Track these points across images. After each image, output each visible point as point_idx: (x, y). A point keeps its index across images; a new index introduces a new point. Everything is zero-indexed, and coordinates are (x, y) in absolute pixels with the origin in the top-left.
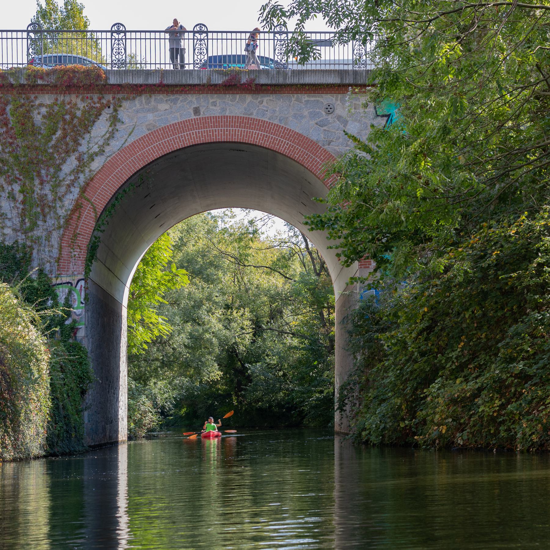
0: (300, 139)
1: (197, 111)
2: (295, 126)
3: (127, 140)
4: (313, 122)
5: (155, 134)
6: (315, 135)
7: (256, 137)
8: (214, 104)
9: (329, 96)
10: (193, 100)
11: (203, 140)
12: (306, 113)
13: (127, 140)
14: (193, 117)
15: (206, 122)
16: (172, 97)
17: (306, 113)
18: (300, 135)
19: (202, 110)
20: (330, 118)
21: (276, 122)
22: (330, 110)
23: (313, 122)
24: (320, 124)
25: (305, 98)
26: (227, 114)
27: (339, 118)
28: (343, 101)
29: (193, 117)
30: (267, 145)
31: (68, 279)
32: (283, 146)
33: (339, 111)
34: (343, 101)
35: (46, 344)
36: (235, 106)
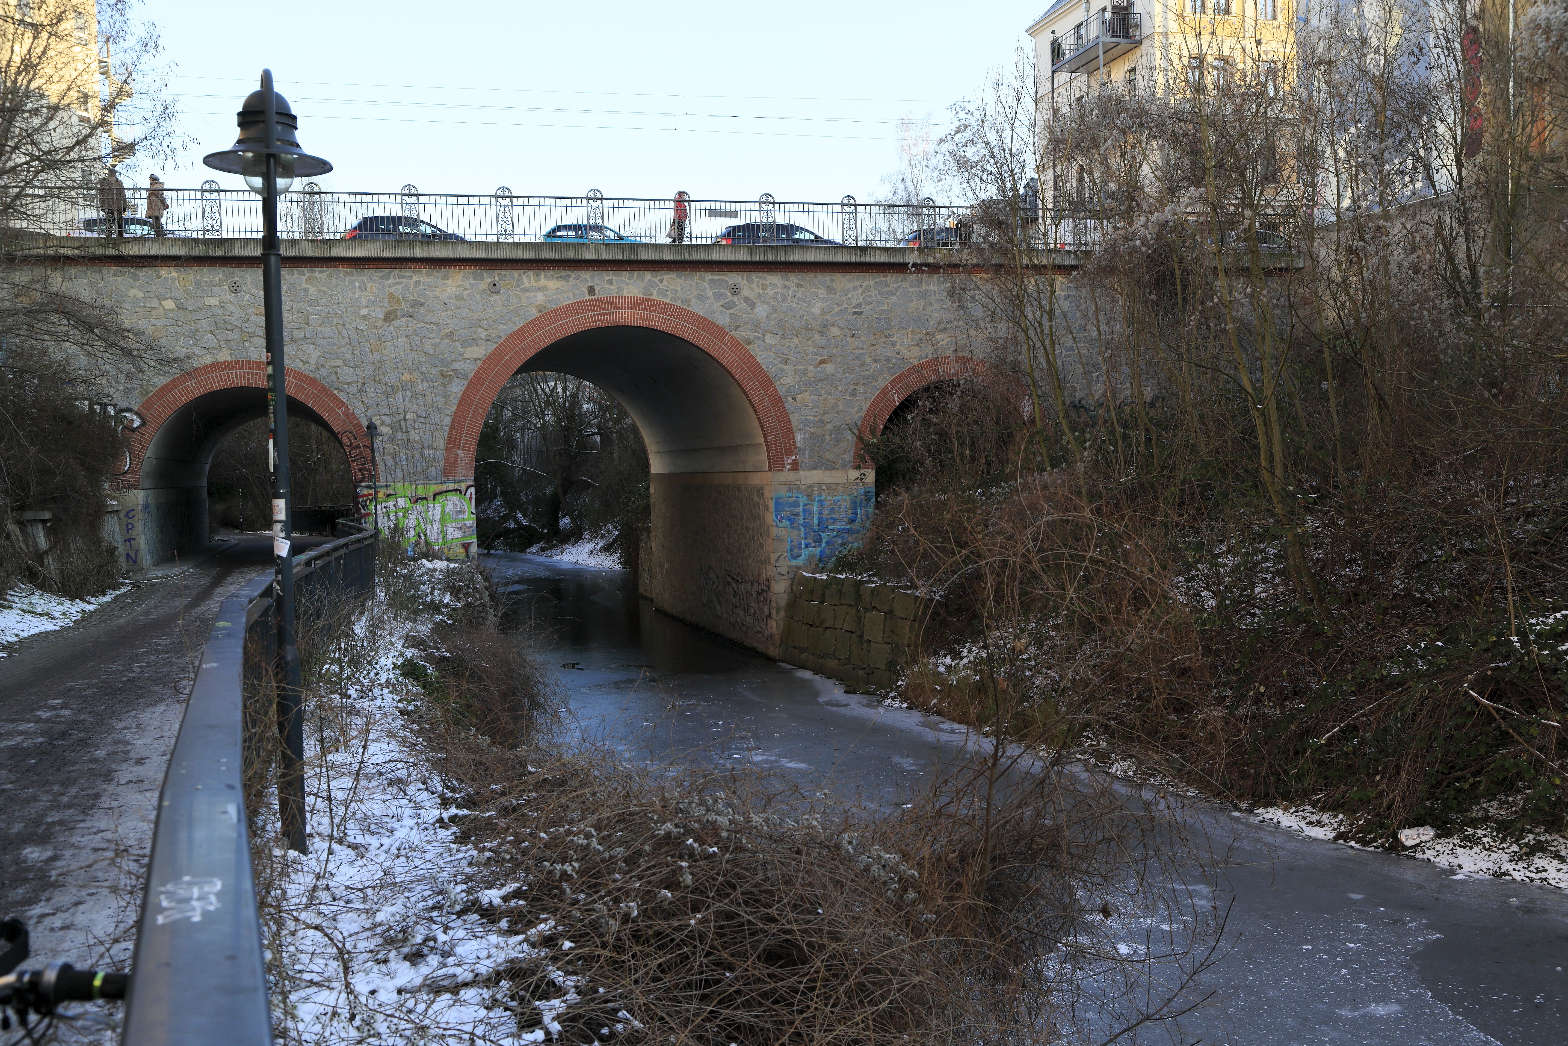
0: (705, 324)
1: (591, 290)
2: (698, 308)
3: (62, 928)
4: (717, 304)
5: (548, 316)
6: (722, 319)
7: (657, 321)
8: (610, 282)
9: (734, 274)
10: (588, 277)
11: (599, 324)
12: (710, 293)
13: (62, 928)
14: (588, 297)
15: (602, 304)
16: (564, 273)
17: (710, 293)
18: (705, 319)
19: (597, 289)
20: (735, 299)
21: (678, 304)
22: (735, 290)
23: (717, 304)
24: (726, 307)
25: (709, 276)
26: (625, 294)
27: (746, 299)
28: (750, 281)
29: (588, 297)
30: (669, 330)
31: (455, 486)
32: (687, 333)
33: (746, 292)
34: (750, 281)
35: (1199, 88)
36: (631, 286)
